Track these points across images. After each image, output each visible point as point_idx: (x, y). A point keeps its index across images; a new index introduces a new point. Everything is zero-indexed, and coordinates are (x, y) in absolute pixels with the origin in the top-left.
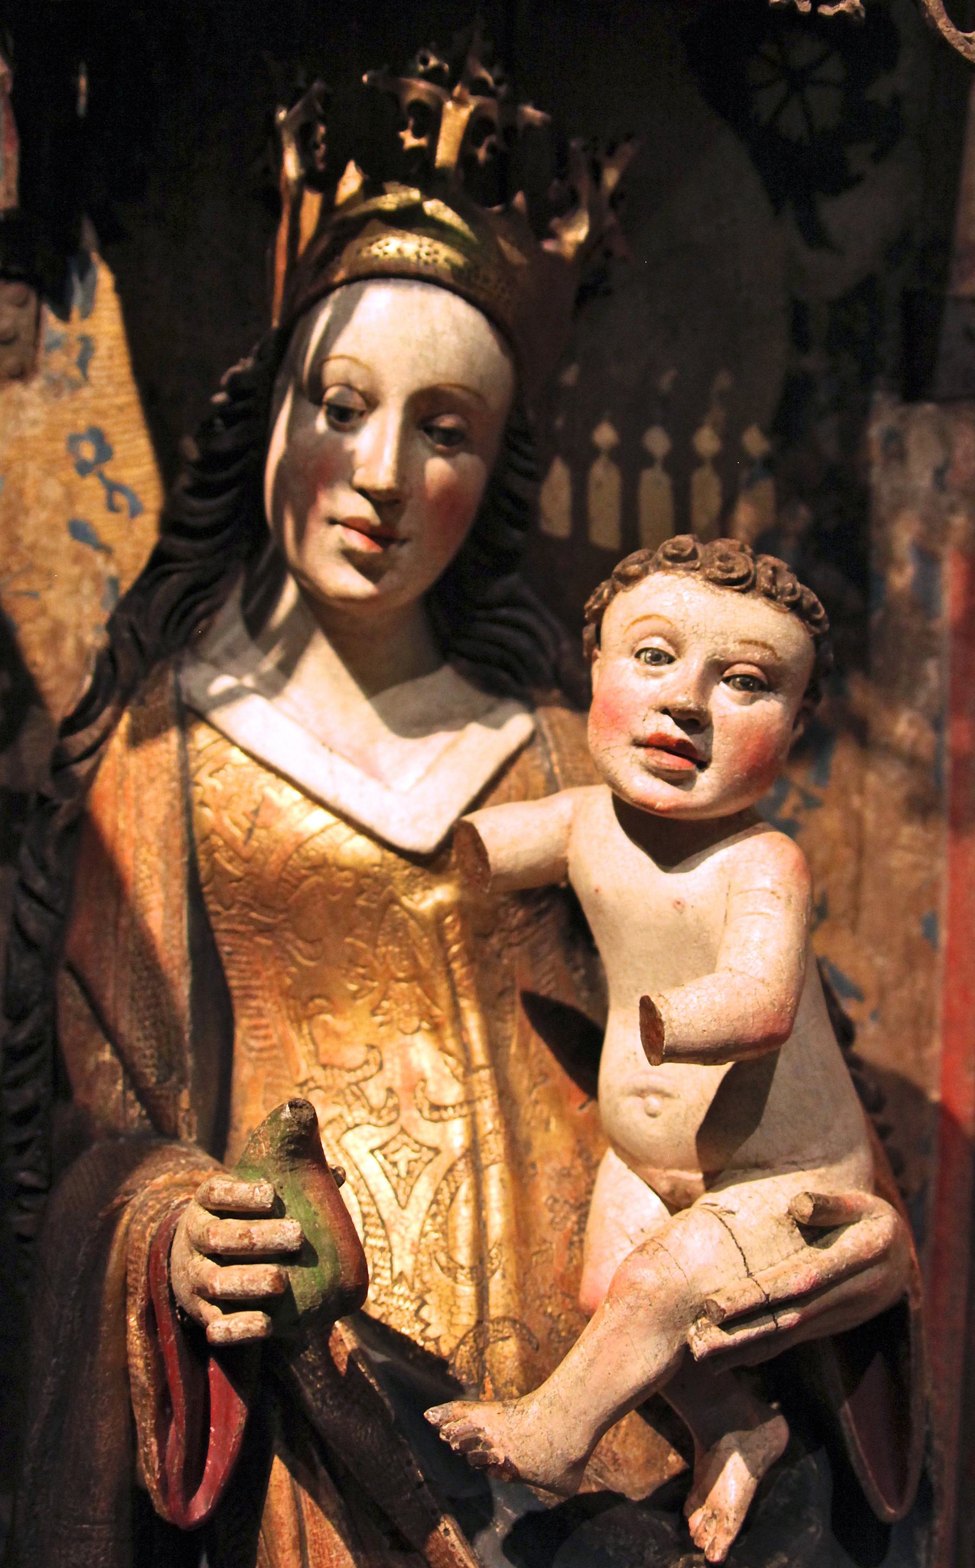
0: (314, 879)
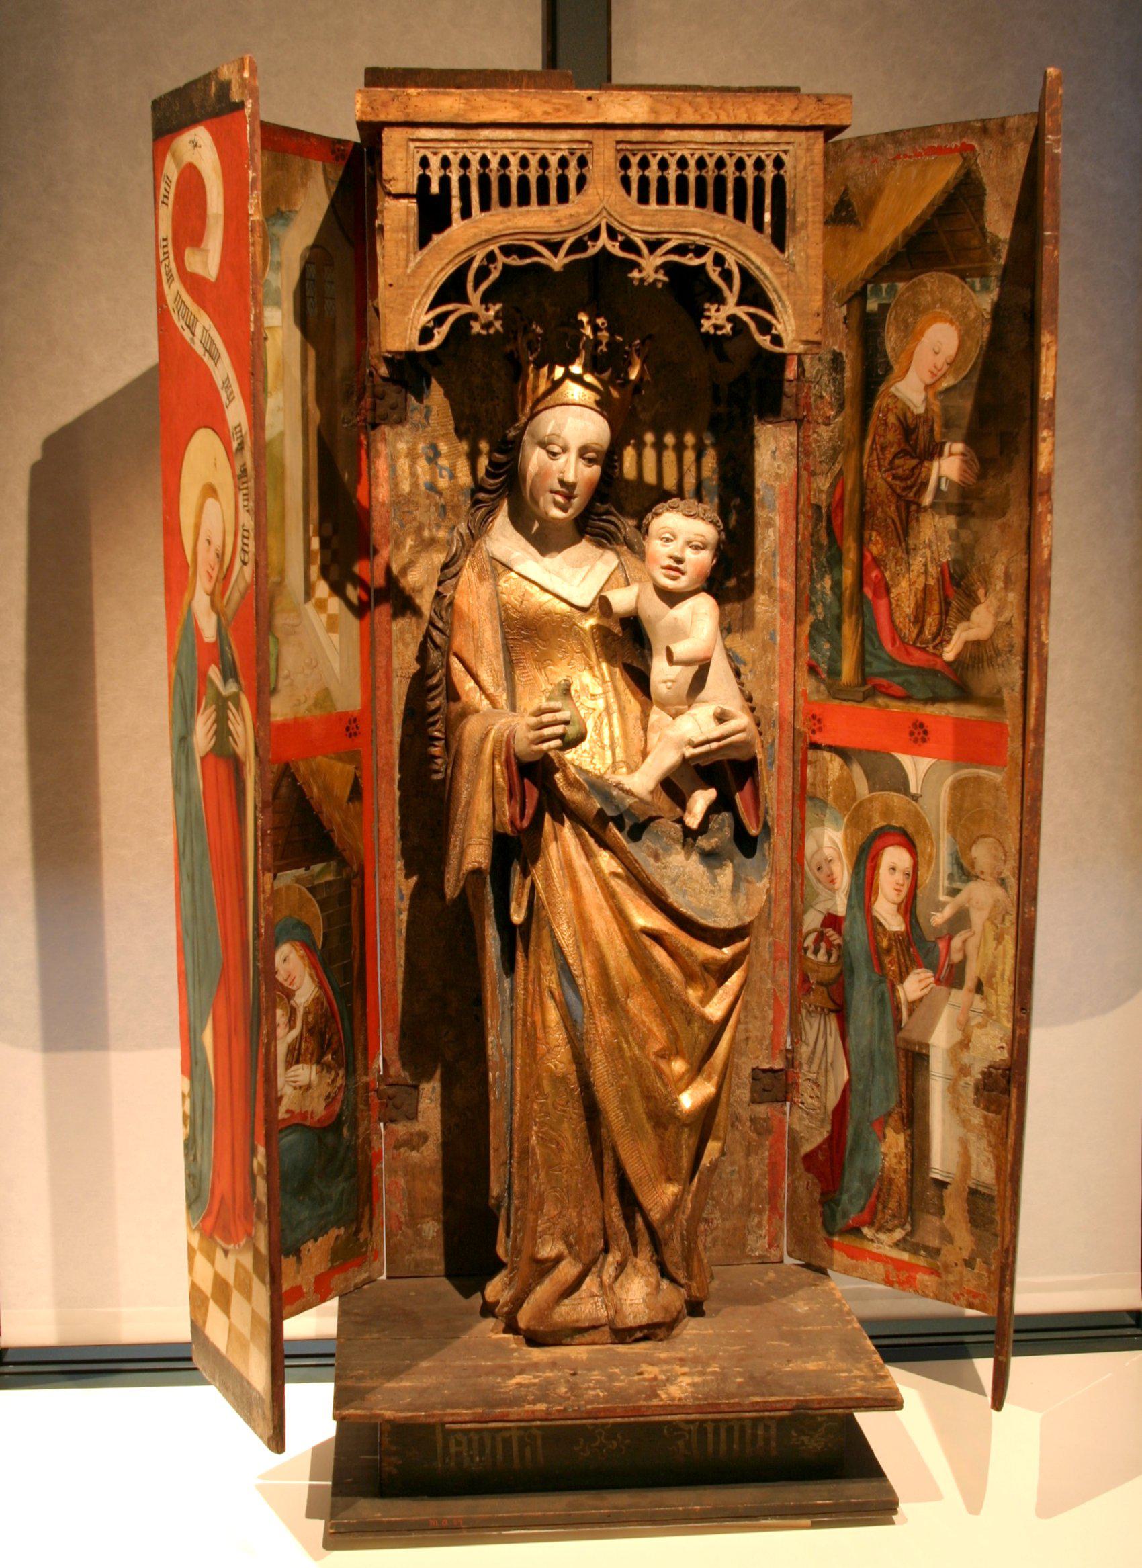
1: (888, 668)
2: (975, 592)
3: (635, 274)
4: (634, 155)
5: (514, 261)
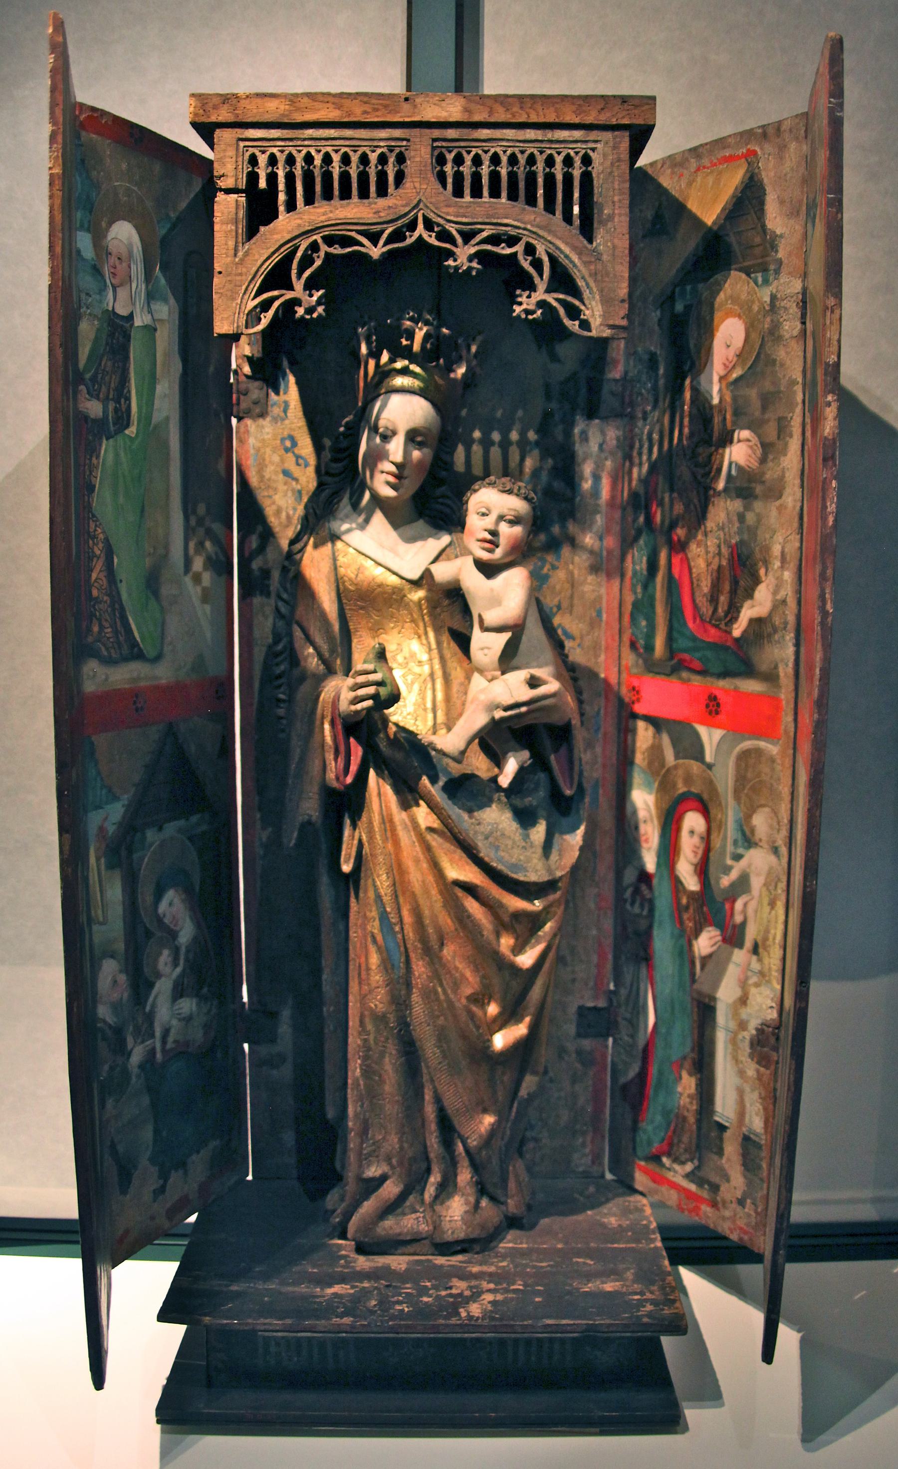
0: (379, 590)
1: (690, 644)
2: (757, 571)
3: (450, 262)
4: (450, 152)
5: (337, 250)
